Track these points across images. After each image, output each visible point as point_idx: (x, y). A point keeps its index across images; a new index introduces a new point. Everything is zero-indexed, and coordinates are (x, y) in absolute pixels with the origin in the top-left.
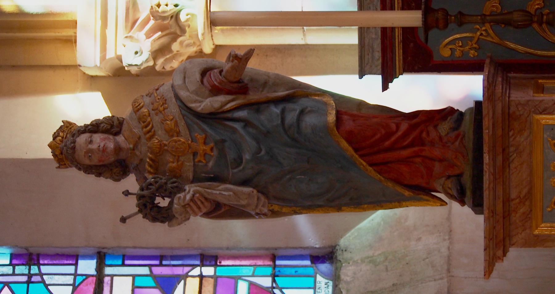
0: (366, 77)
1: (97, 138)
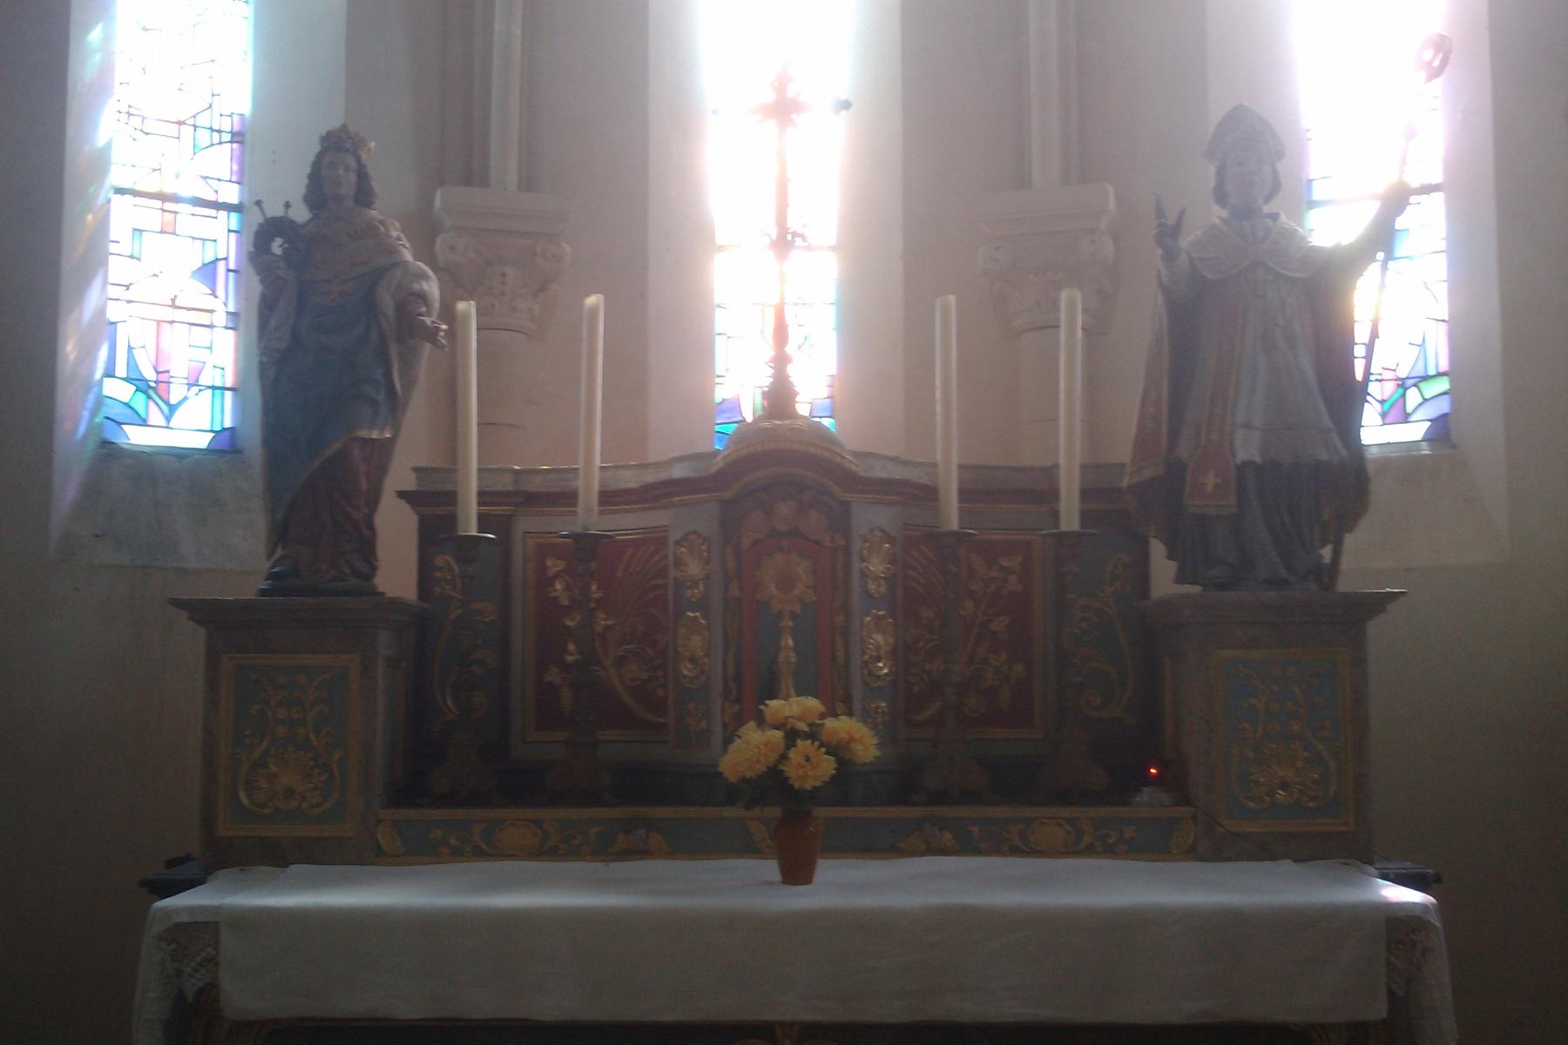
0: (413, 475)
1: (353, 177)
